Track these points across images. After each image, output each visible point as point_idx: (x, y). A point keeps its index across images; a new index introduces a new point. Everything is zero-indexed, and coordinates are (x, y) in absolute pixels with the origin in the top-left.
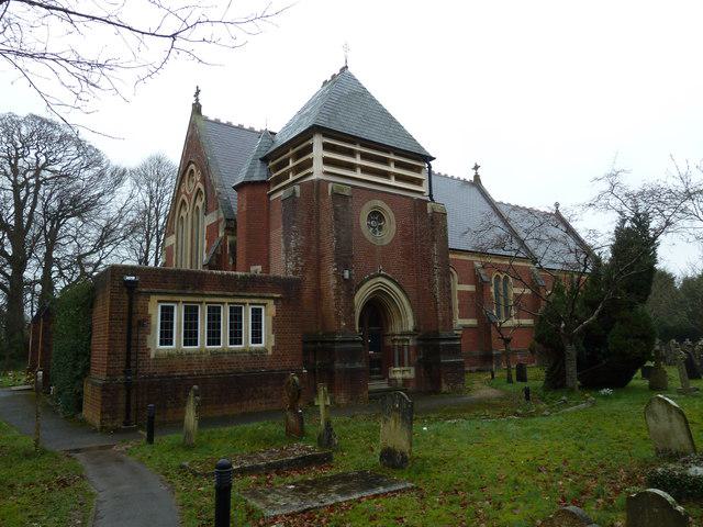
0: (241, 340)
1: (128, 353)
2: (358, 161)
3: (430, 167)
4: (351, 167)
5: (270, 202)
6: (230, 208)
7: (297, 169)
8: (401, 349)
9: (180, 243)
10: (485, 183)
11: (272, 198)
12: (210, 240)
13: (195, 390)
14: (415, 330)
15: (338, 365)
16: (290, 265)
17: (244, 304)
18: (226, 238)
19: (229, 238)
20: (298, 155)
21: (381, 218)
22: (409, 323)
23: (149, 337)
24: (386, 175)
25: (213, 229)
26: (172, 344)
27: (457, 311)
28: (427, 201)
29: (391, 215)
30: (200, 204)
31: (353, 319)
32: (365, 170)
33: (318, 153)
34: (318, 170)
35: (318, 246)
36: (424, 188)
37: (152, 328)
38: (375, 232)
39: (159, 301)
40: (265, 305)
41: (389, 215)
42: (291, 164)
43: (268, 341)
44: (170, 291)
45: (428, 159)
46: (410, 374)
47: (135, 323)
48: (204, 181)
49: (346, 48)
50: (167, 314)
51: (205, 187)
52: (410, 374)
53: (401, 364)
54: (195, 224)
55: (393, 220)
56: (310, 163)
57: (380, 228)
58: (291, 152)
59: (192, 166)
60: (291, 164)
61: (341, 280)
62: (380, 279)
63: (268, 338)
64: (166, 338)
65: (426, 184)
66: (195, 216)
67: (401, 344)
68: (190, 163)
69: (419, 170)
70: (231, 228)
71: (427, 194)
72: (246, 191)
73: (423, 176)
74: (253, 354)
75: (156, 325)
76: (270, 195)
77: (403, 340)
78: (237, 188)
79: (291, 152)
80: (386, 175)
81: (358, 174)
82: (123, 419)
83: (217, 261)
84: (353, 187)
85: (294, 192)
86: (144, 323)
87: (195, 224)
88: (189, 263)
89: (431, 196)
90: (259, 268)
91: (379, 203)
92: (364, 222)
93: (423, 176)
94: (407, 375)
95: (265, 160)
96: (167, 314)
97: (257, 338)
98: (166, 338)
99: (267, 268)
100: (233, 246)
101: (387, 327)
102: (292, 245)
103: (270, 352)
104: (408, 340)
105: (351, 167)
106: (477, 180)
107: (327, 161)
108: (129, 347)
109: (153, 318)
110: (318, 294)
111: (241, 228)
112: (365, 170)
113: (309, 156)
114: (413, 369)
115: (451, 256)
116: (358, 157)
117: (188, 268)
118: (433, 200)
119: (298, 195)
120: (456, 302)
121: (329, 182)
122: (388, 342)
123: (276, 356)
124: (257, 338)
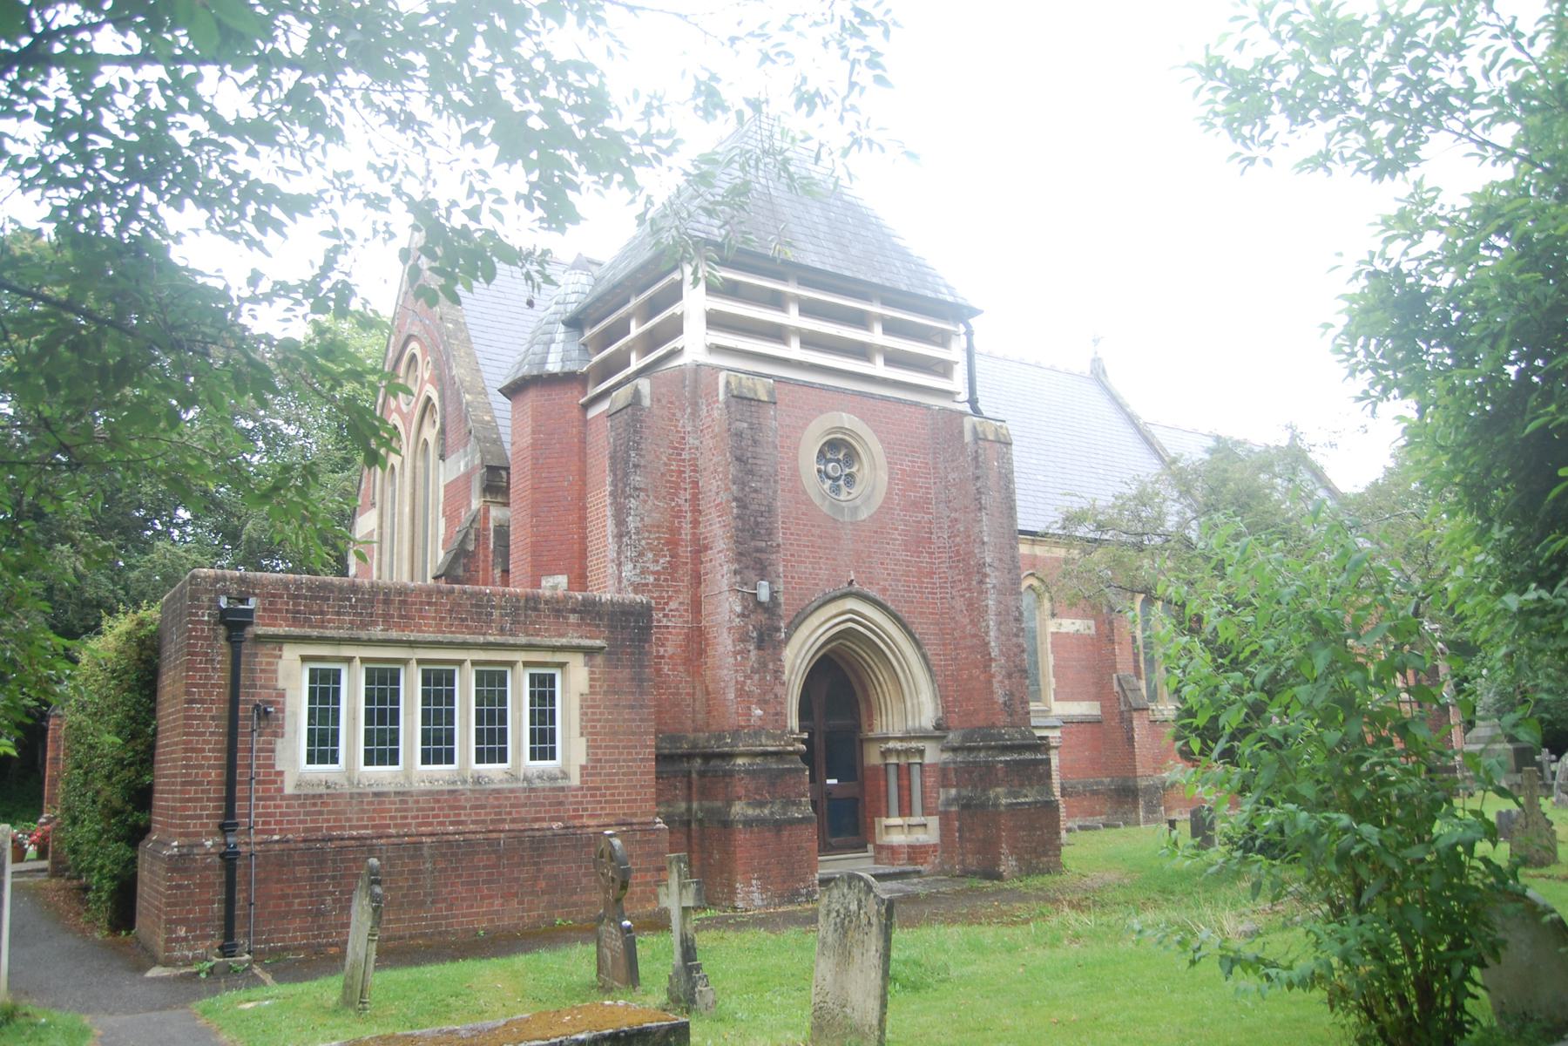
0: (553, 750)
1: (231, 783)
2: (792, 318)
3: (969, 334)
4: (778, 334)
5: (585, 422)
6: (497, 441)
7: (650, 341)
8: (904, 772)
9: (387, 530)
10: (1116, 381)
11: (593, 413)
12: (451, 519)
13: (372, 871)
14: (938, 727)
15: (739, 809)
16: (628, 570)
17: (512, 664)
18: (487, 511)
19: (496, 513)
20: (652, 308)
21: (852, 456)
22: (923, 708)
23: (280, 744)
24: (862, 351)
25: (456, 491)
26: (553, 757)
27: (1049, 682)
28: (963, 414)
29: (876, 447)
30: (430, 433)
31: (780, 702)
32: (811, 341)
33: (695, 304)
34: (695, 344)
35: (695, 523)
36: (958, 383)
37: (288, 728)
38: (836, 490)
39: (305, 659)
40: (562, 665)
41: (872, 447)
42: (635, 330)
43: (572, 750)
44: (328, 633)
45: (960, 313)
46: (930, 834)
47: (244, 709)
48: (440, 380)
49: (1096, 341)
50: (324, 689)
51: (442, 397)
52: (930, 834)
53: (905, 809)
54: (420, 483)
55: (881, 460)
56: (675, 327)
57: (850, 480)
58: (634, 302)
59: (414, 347)
60: (635, 330)
61: (754, 605)
62: (851, 604)
63: (310, 772)
64: (323, 746)
65: (960, 373)
66: (420, 464)
67: (903, 761)
68: (410, 338)
69: (943, 339)
70: (495, 482)
71: (964, 396)
72: (531, 398)
73: (955, 353)
74: (485, 795)
75: (295, 714)
76: (586, 407)
77: (907, 752)
78: (513, 390)
79: (634, 302)
80: (862, 351)
81: (794, 351)
82: (218, 941)
83: (461, 564)
84: (780, 380)
85: (637, 394)
86: (268, 716)
87: (420, 483)
88: (406, 567)
89: (973, 401)
90: (562, 581)
91: (848, 420)
92: (809, 462)
93: (955, 353)
94: (920, 837)
95: (575, 323)
96: (324, 689)
97: (543, 745)
98: (323, 746)
99: (580, 579)
100: (502, 532)
101: (870, 716)
102: (632, 523)
103: (575, 781)
104: (921, 752)
105: (778, 334)
106: (1098, 375)
107: (716, 321)
108: (231, 767)
109: (289, 700)
110: (697, 640)
111: (519, 483)
112: (811, 341)
113: (676, 309)
114: (933, 822)
115: (1024, 549)
116: (794, 310)
117: (405, 579)
118: (977, 411)
119: (646, 402)
120: (1048, 661)
121: (722, 369)
122: (873, 757)
123: (587, 788)
124: (543, 745)
